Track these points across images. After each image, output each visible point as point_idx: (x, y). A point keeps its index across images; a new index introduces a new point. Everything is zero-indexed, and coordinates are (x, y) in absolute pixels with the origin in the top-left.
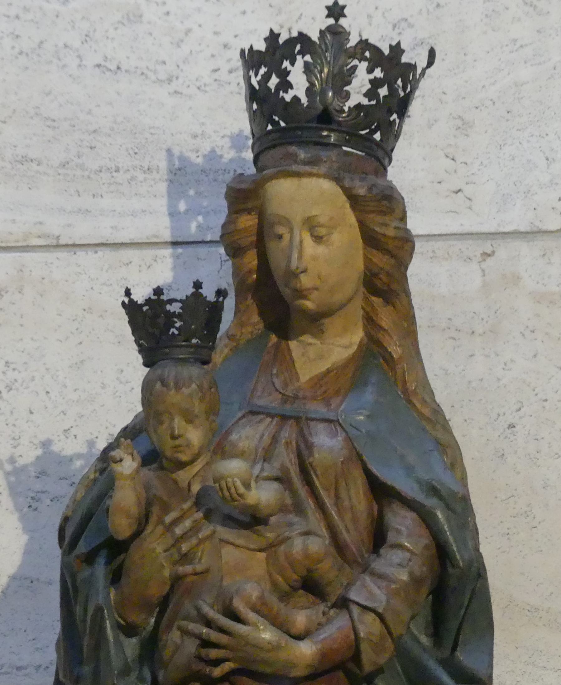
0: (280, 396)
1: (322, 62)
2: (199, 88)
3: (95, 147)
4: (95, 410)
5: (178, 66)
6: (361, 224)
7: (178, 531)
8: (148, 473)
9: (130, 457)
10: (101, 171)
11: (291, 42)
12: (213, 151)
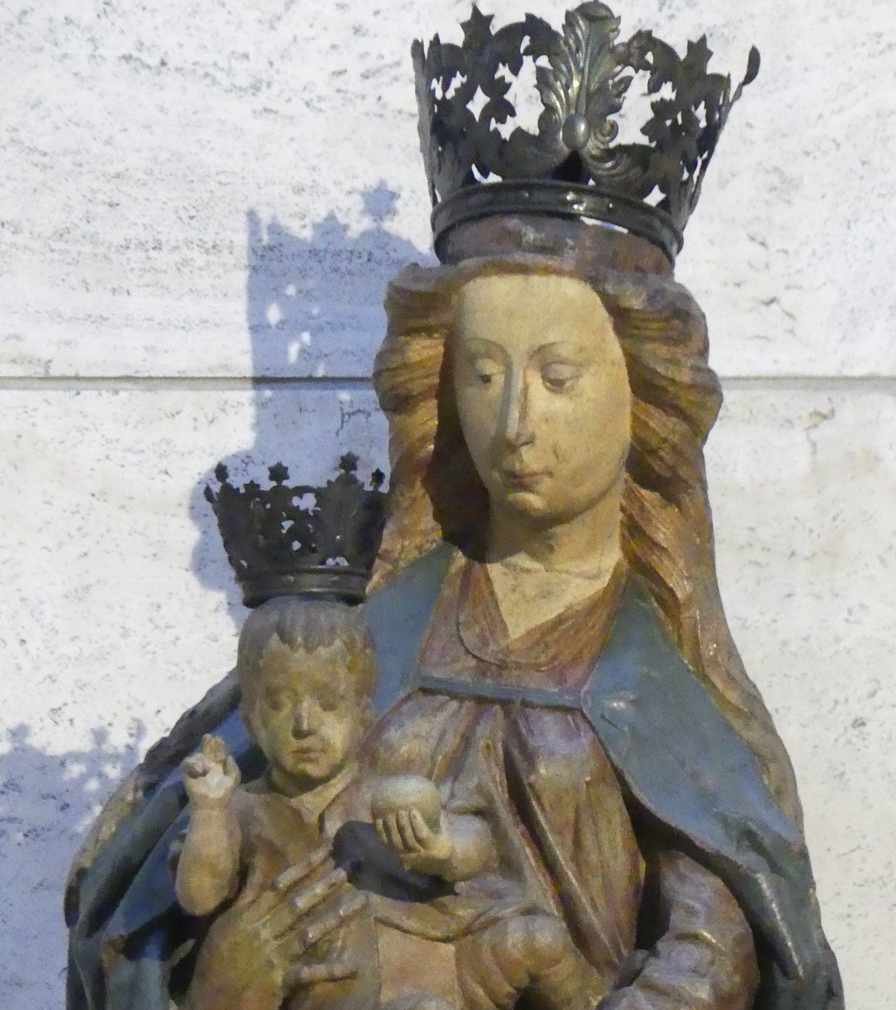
0: (473, 663)
1: (569, 70)
2: (308, 104)
3: (118, 205)
4: (108, 675)
5: (271, 63)
6: (633, 362)
7: (302, 902)
8: (253, 799)
9: (219, 768)
10: (128, 248)
11: (513, 32)
12: (331, 217)
